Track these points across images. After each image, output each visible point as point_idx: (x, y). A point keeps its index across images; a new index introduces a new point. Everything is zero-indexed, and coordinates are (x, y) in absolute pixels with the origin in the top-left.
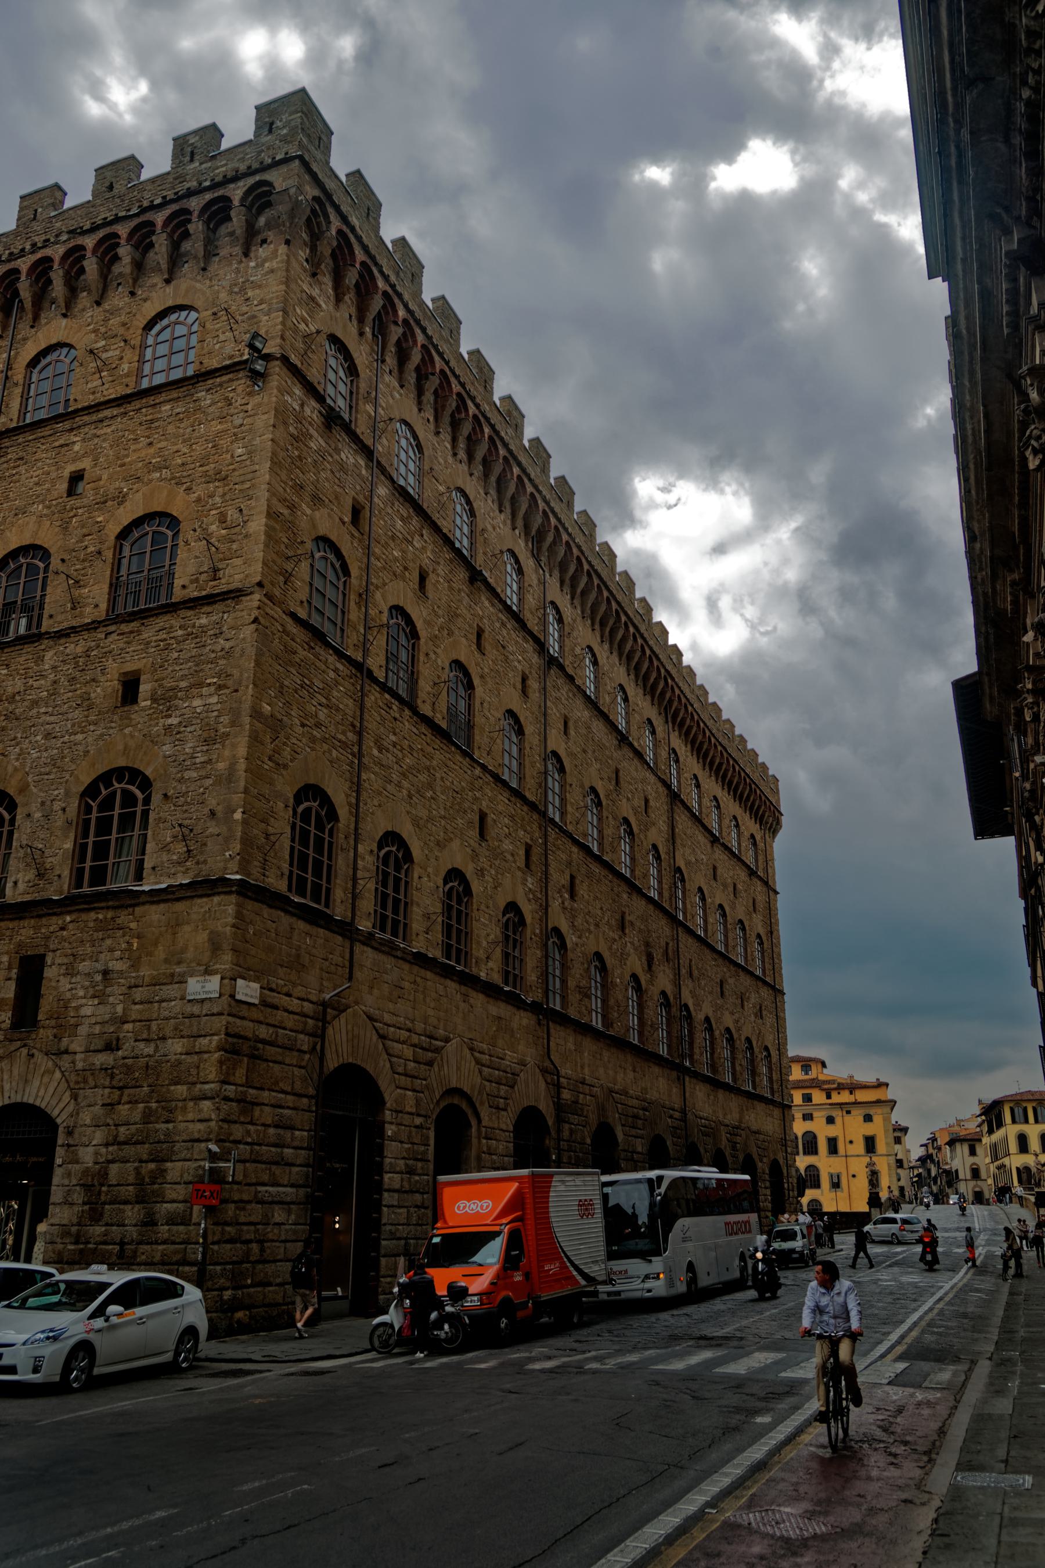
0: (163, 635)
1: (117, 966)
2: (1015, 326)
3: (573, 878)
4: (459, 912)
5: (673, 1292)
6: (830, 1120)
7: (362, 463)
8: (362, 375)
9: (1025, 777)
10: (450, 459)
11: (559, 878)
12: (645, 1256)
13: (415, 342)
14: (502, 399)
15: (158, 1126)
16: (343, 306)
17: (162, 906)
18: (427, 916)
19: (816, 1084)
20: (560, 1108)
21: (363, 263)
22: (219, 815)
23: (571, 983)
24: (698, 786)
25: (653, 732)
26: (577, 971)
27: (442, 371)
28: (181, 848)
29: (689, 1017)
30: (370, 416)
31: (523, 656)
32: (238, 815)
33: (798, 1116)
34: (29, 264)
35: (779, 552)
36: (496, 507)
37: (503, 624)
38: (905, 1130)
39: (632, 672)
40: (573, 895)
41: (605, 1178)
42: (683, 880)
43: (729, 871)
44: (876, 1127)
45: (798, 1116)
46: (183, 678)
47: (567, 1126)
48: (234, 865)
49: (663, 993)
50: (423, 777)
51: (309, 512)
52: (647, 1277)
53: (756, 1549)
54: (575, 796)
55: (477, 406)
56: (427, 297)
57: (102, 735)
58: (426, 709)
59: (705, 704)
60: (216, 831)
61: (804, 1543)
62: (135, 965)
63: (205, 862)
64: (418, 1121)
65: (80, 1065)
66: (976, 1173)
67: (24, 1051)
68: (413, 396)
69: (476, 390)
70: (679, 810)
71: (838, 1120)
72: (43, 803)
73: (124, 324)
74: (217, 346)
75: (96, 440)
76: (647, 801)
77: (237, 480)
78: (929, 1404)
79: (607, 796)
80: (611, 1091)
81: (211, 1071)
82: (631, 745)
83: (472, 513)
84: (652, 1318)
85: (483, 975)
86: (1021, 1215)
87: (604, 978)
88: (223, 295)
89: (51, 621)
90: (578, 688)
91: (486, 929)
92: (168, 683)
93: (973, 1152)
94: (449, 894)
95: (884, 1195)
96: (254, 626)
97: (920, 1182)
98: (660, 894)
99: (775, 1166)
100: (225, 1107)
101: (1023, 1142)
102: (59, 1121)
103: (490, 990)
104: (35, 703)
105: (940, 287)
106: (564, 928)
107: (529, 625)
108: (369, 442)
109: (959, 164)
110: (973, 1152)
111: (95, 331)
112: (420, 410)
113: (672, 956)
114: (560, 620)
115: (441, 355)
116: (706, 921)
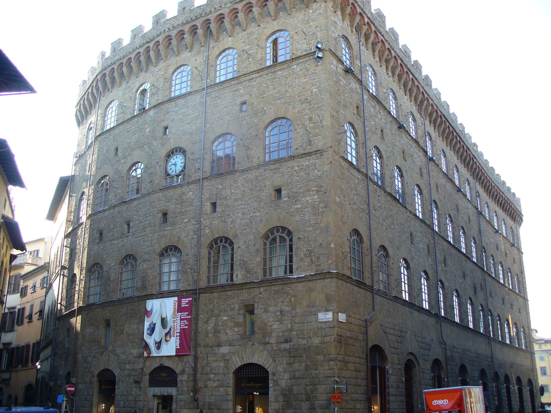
0: (289, 170)
1: (286, 308)
7: (358, 87)
8: (354, 49)
10: (386, 76)
11: (440, 258)
13: (371, 30)
14: (402, 46)
15: (311, 372)
16: (345, 22)
17: (303, 284)
20: (446, 357)
22: (324, 245)
28: (308, 260)
30: (358, 66)
32: (332, 246)
34: (214, 17)
36: (403, 94)
39: (459, 158)
46: (301, 188)
48: (333, 266)
51: (343, 113)
57: (267, 213)
59: (476, 151)
60: (324, 252)
62: (294, 308)
63: (320, 265)
65: (275, 348)
67: (251, 343)
68: (371, 52)
70: (481, 219)
71: (546, 359)
72: (245, 242)
73: (256, 39)
74: (299, 46)
75: (250, 88)
77: (315, 102)
79: (454, 217)
81: (333, 351)
85: (416, 303)
88: (299, 25)
89: (239, 165)
92: (295, 190)
96: (330, 165)
100: (339, 364)
102: (269, 370)
104: (236, 200)
107: (420, 143)
111: (244, 42)
112: (374, 58)
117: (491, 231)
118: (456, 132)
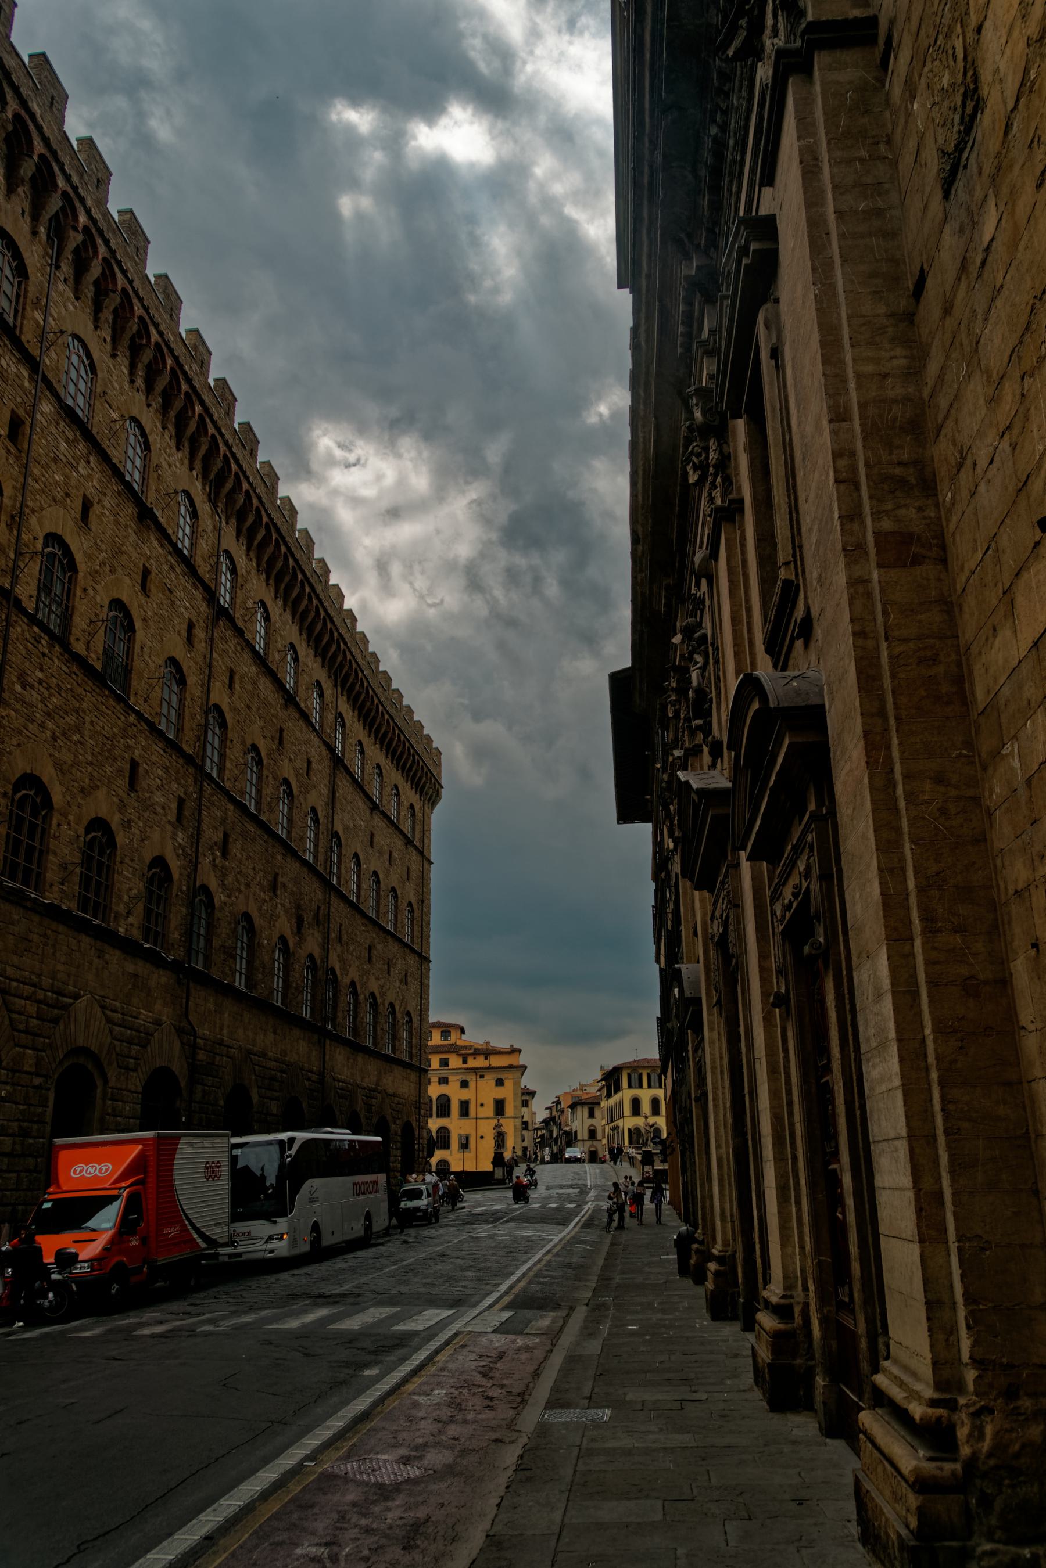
2: (687, 348)
3: (226, 836)
4: (100, 864)
5: (296, 1251)
6: (464, 1084)
9: (664, 768)
10: (126, 386)
11: (211, 835)
12: (270, 1217)
18: (64, 866)
19: (454, 1049)
21: (41, 156)
23: (216, 943)
24: (362, 752)
25: (321, 695)
26: (224, 929)
27: (124, 290)
29: (335, 981)
31: (190, 603)
33: (434, 1080)
35: (457, 523)
36: (173, 444)
37: (172, 567)
38: (532, 1094)
40: (225, 853)
41: (235, 1140)
42: (339, 845)
43: (385, 838)
44: (507, 1092)
45: (434, 1080)
47: (200, 1088)
49: (311, 956)
50: (71, 719)
52: (271, 1238)
53: (350, 1497)
54: (235, 753)
55: (161, 334)
56: (114, 207)
58: (79, 648)
59: (375, 672)
61: (397, 1487)
64: (37, 1081)
66: (592, 1134)
69: (161, 317)
70: (341, 775)
71: (472, 1084)
76: (309, 763)
78: (527, 1348)
79: (269, 755)
80: (249, 1052)
82: (297, 706)
83: (147, 446)
84: (272, 1279)
86: (628, 1172)
87: (251, 940)
90: (247, 642)
91: (129, 882)
93: (591, 1115)
94: (90, 845)
95: (508, 1155)
97: (542, 1143)
98: (316, 857)
99: (407, 1128)
101: (636, 1103)
103: (128, 947)
105: (626, 297)
106: (213, 884)
108: (35, 352)
109: (650, 184)
110: (591, 1115)
112: (96, 328)
113: (322, 920)
114: (234, 571)
115: (124, 272)
116: (359, 887)
117: (361, 804)
118: (357, 662)
